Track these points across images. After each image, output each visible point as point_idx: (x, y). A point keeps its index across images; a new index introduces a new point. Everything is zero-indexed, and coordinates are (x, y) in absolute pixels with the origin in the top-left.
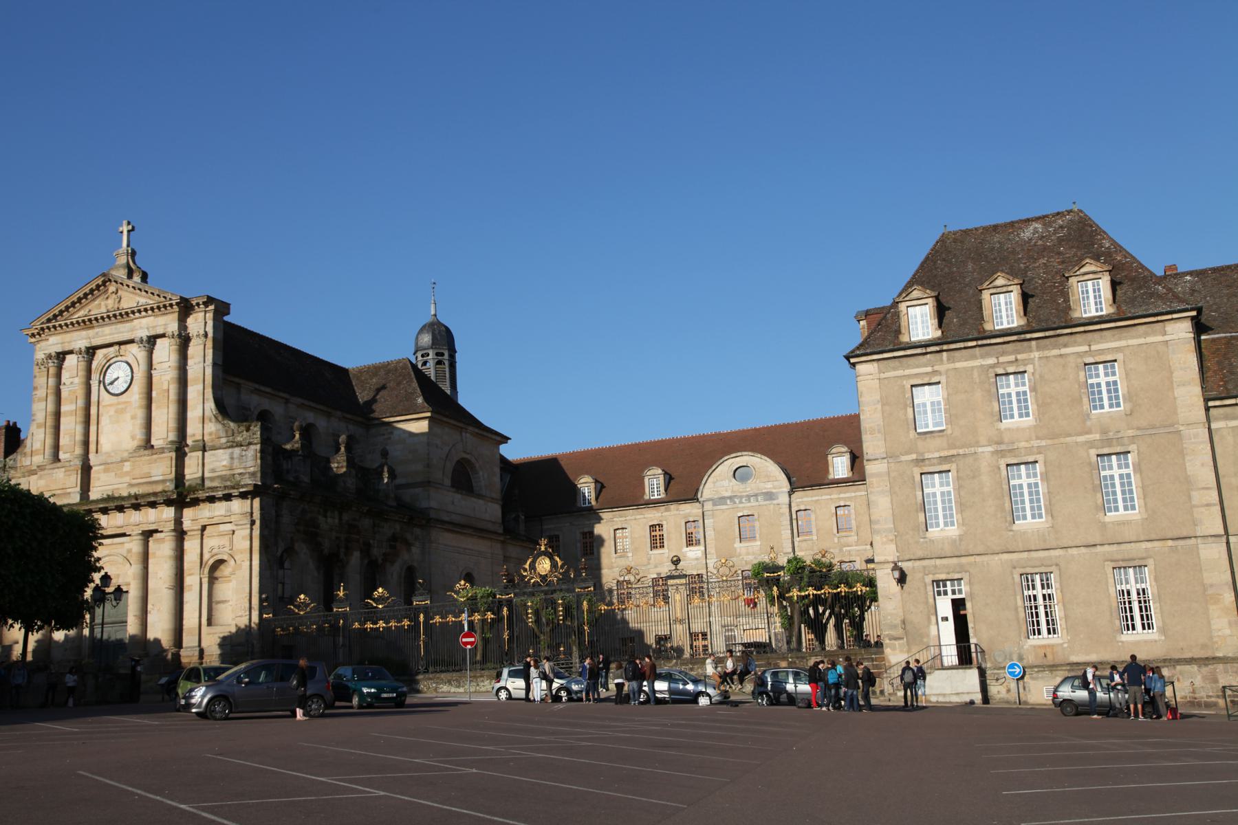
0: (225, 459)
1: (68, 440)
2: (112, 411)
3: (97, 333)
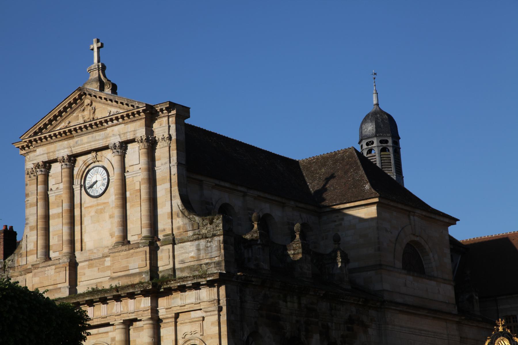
0: (193, 251)
1: (57, 240)
2: (93, 213)
3: (76, 142)
